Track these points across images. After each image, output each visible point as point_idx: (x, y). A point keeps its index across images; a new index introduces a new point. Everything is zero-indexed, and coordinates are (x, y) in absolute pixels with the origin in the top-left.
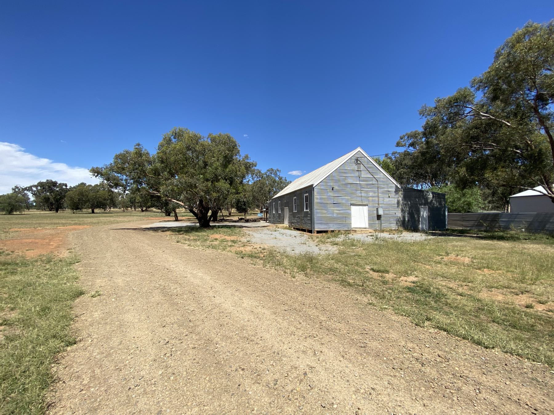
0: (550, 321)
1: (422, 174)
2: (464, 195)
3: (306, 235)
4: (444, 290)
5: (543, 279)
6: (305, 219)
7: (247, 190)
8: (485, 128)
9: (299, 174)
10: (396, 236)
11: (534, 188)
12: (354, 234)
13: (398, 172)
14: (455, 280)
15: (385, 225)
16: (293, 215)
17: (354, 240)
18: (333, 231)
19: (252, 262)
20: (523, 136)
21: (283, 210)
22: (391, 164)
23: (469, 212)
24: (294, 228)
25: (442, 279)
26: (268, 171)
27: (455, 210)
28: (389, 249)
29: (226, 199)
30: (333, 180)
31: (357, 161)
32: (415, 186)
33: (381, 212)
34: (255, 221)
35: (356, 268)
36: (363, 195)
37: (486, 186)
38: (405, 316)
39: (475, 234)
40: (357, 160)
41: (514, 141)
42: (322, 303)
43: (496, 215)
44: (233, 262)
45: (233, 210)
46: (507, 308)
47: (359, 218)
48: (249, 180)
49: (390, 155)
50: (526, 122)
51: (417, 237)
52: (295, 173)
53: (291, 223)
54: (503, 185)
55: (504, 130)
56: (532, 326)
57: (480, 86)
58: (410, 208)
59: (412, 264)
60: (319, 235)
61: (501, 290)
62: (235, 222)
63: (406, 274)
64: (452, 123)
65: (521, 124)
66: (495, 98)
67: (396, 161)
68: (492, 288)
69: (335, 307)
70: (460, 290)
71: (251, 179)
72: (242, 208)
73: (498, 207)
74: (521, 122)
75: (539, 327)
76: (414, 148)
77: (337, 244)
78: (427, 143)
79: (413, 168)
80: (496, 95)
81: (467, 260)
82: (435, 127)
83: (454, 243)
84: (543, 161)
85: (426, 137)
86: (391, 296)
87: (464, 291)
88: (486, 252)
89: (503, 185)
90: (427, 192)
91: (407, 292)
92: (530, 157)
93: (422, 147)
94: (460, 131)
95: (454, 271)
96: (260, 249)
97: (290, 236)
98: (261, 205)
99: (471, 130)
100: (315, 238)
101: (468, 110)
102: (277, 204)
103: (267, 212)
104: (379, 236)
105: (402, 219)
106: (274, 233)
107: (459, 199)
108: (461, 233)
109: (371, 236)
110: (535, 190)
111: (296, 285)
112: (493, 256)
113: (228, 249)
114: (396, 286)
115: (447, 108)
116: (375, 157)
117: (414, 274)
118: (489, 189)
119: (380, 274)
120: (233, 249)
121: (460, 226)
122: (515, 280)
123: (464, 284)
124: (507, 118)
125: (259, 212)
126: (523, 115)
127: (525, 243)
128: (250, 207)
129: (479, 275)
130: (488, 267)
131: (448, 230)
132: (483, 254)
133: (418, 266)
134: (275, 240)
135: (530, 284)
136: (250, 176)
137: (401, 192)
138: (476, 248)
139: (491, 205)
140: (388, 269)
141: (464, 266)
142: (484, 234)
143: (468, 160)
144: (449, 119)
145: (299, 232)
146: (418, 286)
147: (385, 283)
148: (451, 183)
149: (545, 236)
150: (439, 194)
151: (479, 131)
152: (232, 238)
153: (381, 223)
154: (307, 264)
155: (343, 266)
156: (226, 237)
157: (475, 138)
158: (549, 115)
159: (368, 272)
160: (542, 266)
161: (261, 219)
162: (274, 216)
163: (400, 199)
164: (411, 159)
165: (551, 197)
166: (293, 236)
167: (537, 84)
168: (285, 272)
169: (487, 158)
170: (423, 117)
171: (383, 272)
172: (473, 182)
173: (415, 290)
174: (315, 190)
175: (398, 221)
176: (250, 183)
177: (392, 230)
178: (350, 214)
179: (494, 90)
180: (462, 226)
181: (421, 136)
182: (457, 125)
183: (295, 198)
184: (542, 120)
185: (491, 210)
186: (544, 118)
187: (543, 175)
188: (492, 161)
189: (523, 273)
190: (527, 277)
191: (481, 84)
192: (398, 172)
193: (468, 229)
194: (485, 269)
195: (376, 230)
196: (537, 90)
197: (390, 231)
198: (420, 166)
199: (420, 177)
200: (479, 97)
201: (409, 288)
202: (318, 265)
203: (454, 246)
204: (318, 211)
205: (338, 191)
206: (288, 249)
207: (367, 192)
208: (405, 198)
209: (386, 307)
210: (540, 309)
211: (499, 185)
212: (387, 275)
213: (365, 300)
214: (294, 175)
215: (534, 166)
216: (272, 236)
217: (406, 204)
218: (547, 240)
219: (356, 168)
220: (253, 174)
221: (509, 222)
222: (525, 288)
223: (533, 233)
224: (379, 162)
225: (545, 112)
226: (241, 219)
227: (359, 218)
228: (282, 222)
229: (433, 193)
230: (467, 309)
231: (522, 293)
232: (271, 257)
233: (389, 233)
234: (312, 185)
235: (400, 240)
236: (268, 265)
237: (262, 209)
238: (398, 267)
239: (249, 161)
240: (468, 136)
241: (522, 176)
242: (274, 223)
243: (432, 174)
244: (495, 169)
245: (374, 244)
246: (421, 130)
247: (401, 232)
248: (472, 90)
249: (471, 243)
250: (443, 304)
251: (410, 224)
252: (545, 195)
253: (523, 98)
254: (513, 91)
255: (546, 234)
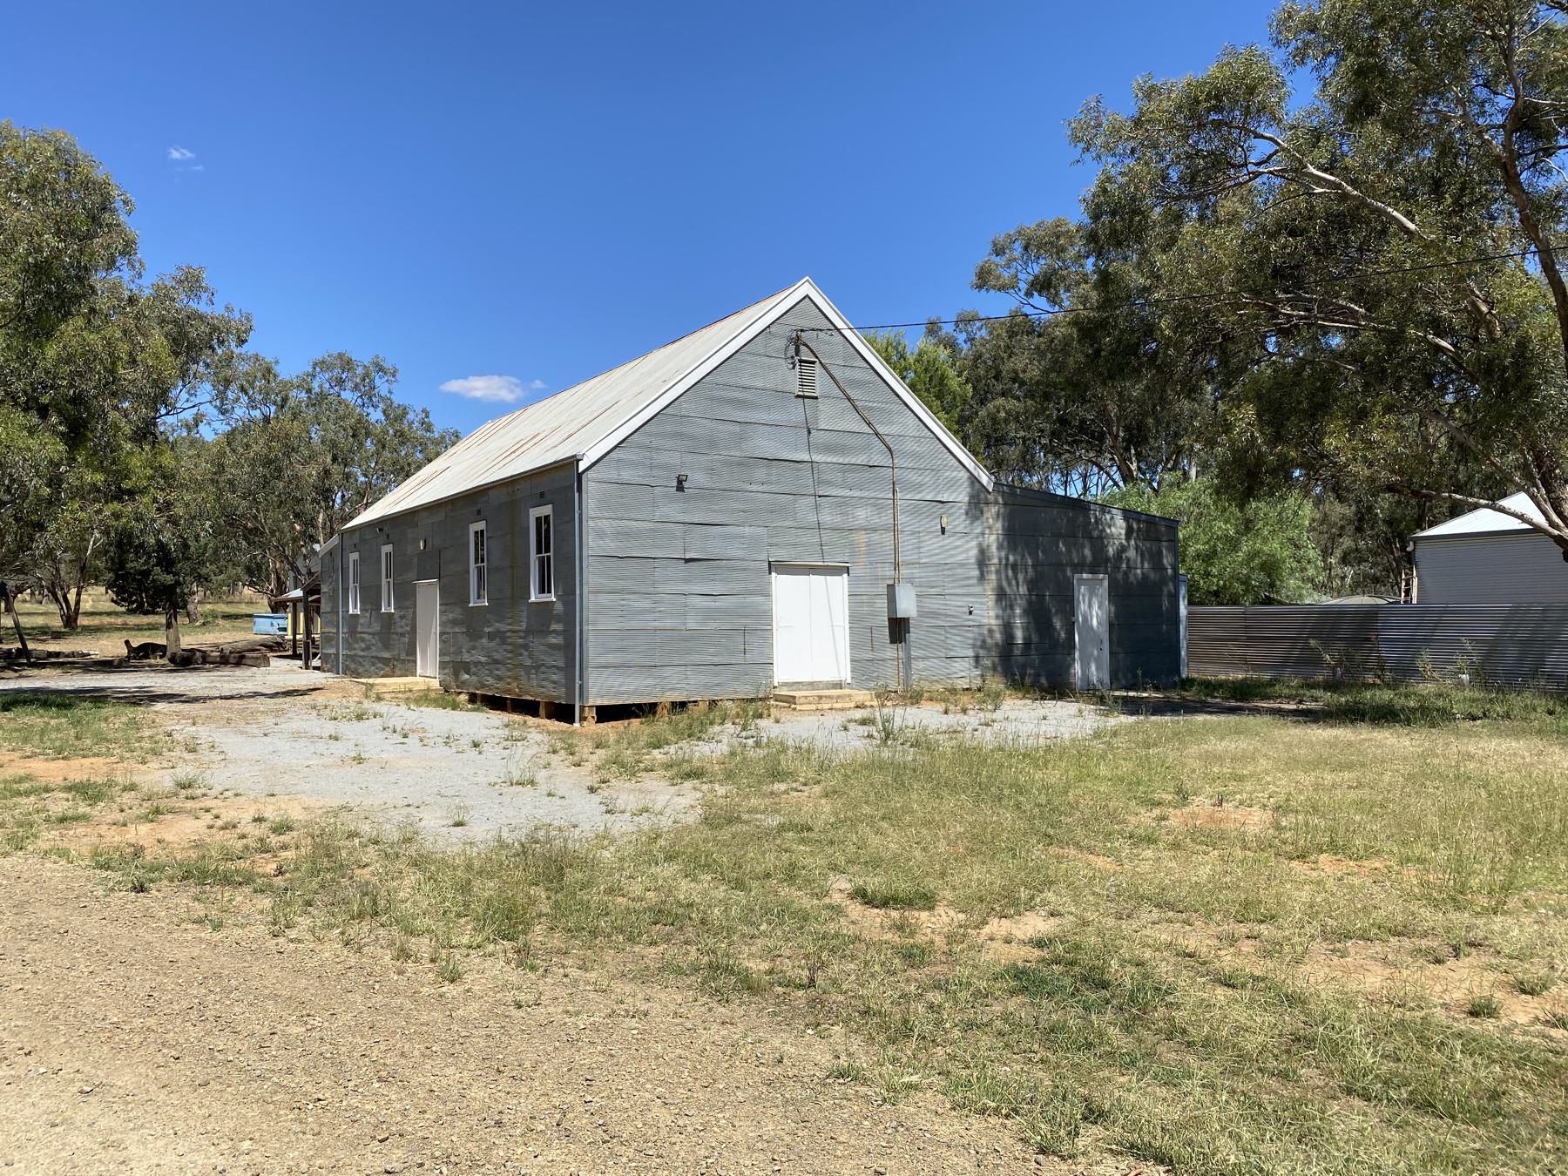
0: (1558, 1068)
1: (1083, 427)
2: (1248, 526)
3: (540, 731)
4: (1163, 967)
5: (1529, 887)
6: (536, 643)
7: (183, 474)
8: (1324, 234)
9: (508, 396)
10: (972, 719)
11: (1504, 503)
12: (785, 716)
13: (983, 413)
14: (1208, 917)
15: (926, 669)
16: (465, 625)
17: (784, 750)
18: (683, 705)
19: (199, 910)
20: (1462, 279)
21: (406, 596)
22: (952, 373)
23: (1268, 601)
24: (473, 698)
25: (1156, 914)
26: (322, 365)
27: (1216, 594)
28: (939, 785)
29: (41, 527)
30: (681, 435)
31: (798, 345)
32: (1056, 478)
33: (907, 606)
34: (236, 659)
35: (785, 891)
36: (827, 518)
37: (1333, 489)
38: (997, 1111)
39: (1290, 698)
40: (797, 342)
41: (1428, 298)
42: (598, 1102)
43: (1370, 614)
44: (76, 920)
45: (96, 598)
46: (1401, 1025)
47: (810, 631)
48: (199, 416)
49: (947, 329)
50: (1473, 222)
51: (1066, 720)
52: (479, 387)
53: (454, 667)
54: (1391, 488)
55: (1394, 249)
56: (1495, 1096)
57: (1307, 45)
58: (1033, 585)
59: (1038, 851)
60: (610, 729)
61: (1378, 947)
62: (107, 666)
63: (1010, 903)
64: (1199, 198)
65: (1456, 230)
66: (1360, 110)
67: (978, 356)
68: (1348, 937)
69: (665, 1117)
70: (1227, 961)
71: (210, 410)
72: (151, 581)
73: (1376, 580)
74: (1456, 220)
75: (1520, 1098)
76: (1054, 300)
77: (696, 774)
78: (1105, 280)
79: (1047, 397)
80: (1366, 95)
81: (1256, 821)
82: (1135, 212)
83: (1214, 740)
84: (1530, 389)
85: (1099, 255)
86: (939, 1023)
87: (1239, 962)
88: (1329, 778)
89: (1391, 488)
90: (1104, 508)
91: (1013, 993)
92: (1487, 370)
93: (1084, 300)
94: (1231, 238)
95: (1205, 872)
96: (255, 831)
97: (448, 741)
98: (273, 564)
99: (1273, 236)
100: (584, 749)
101: (1261, 149)
102: (370, 560)
103: (311, 607)
104: (897, 723)
105: (998, 636)
106: (349, 729)
107: (1233, 545)
108: (1240, 698)
109: (864, 722)
110: (1502, 510)
111: (464, 1021)
112: (1352, 795)
113: (49, 837)
114: (962, 971)
115: (1181, 128)
116: (883, 336)
117: (1044, 903)
118: (1341, 499)
119: (895, 914)
120: (81, 839)
121: (1232, 664)
122: (1430, 898)
123: (1243, 929)
124: (1405, 196)
125: (263, 605)
126: (1462, 189)
127: (1469, 734)
128: (202, 579)
129: (1308, 883)
130: (1333, 848)
131: (1187, 683)
132: (1317, 787)
133: (1059, 859)
134: (357, 768)
135: (1485, 911)
136: (206, 391)
137: (994, 510)
138: (1292, 763)
139: (1350, 571)
140: (931, 884)
141: (1244, 848)
142: (1326, 698)
143: (1264, 370)
144: (1191, 179)
145: (497, 718)
146: (1057, 961)
147: (913, 957)
148: (1204, 468)
149: (1542, 703)
150: (1151, 520)
151: (1300, 243)
152: (80, 769)
153: (909, 658)
154: (535, 898)
155: (721, 892)
156: (38, 766)
157: (1287, 275)
158: (1558, 196)
159: (837, 910)
160: (1528, 830)
161: (276, 647)
162: (353, 631)
163: (992, 540)
164: (1040, 353)
165: (1559, 540)
166: (465, 743)
167: (1519, 64)
168: (404, 954)
169: (1335, 369)
170: (1088, 157)
171: (907, 903)
172: (1282, 469)
173: (1043, 981)
174: (590, 487)
175: (984, 645)
176: (207, 433)
177: (953, 691)
178: (766, 616)
179: (1360, 72)
180: (1245, 662)
181: (1079, 246)
182: (1222, 213)
183: (481, 526)
184: (1535, 215)
185: (1353, 592)
186: (1539, 208)
187: (1532, 448)
188: (1351, 380)
189: (1459, 866)
190: (1474, 882)
191: (1310, 38)
192: (983, 413)
193: (1267, 676)
194: (1323, 857)
195: (883, 695)
196: (1516, 88)
197: (949, 696)
198: (1077, 389)
199: (1076, 437)
200: (1305, 94)
201: (1019, 974)
202: (594, 897)
203: (1210, 758)
204: (604, 599)
205: (707, 494)
206: (432, 823)
207: (843, 504)
208: (1015, 536)
209: (915, 1079)
210: (1522, 1019)
211: (1375, 488)
212: (924, 915)
213: (816, 1053)
214: (477, 401)
215: (1497, 408)
216: (339, 749)
217: (1014, 567)
218: (1549, 719)
219: (791, 380)
220: (227, 382)
221: (1414, 644)
222: (1469, 929)
223: (1500, 690)
224: (902, 356)
225: (1548, 184)
226: (147, 650)
227: (810, 631)
228: (404, 663)
229: (1128, 514)
230: (1251, 1043)
231: (1457, 952)
232: (326, 876)
233: (941, 707)
234: (574, 461)
235: (988, 737)
236: (304, 922)
237: (281, 587)
238: (977, 874)
239: (202, 307)
240: (1260, 264)
241: (1462, 451)
242: (352, 669)
243: (1127, 429)
244: (1362, 415)
245: (875, 765)
246: (1076, 217)
247: (996, 698)
248: (1278, 57)
249: (1273, 742)
250: (1158, 1032)
251: (1033, 664)
252: (1537, 529)
253: (1465, 115)
254: (1430, 87)
255: (1545, 693)
